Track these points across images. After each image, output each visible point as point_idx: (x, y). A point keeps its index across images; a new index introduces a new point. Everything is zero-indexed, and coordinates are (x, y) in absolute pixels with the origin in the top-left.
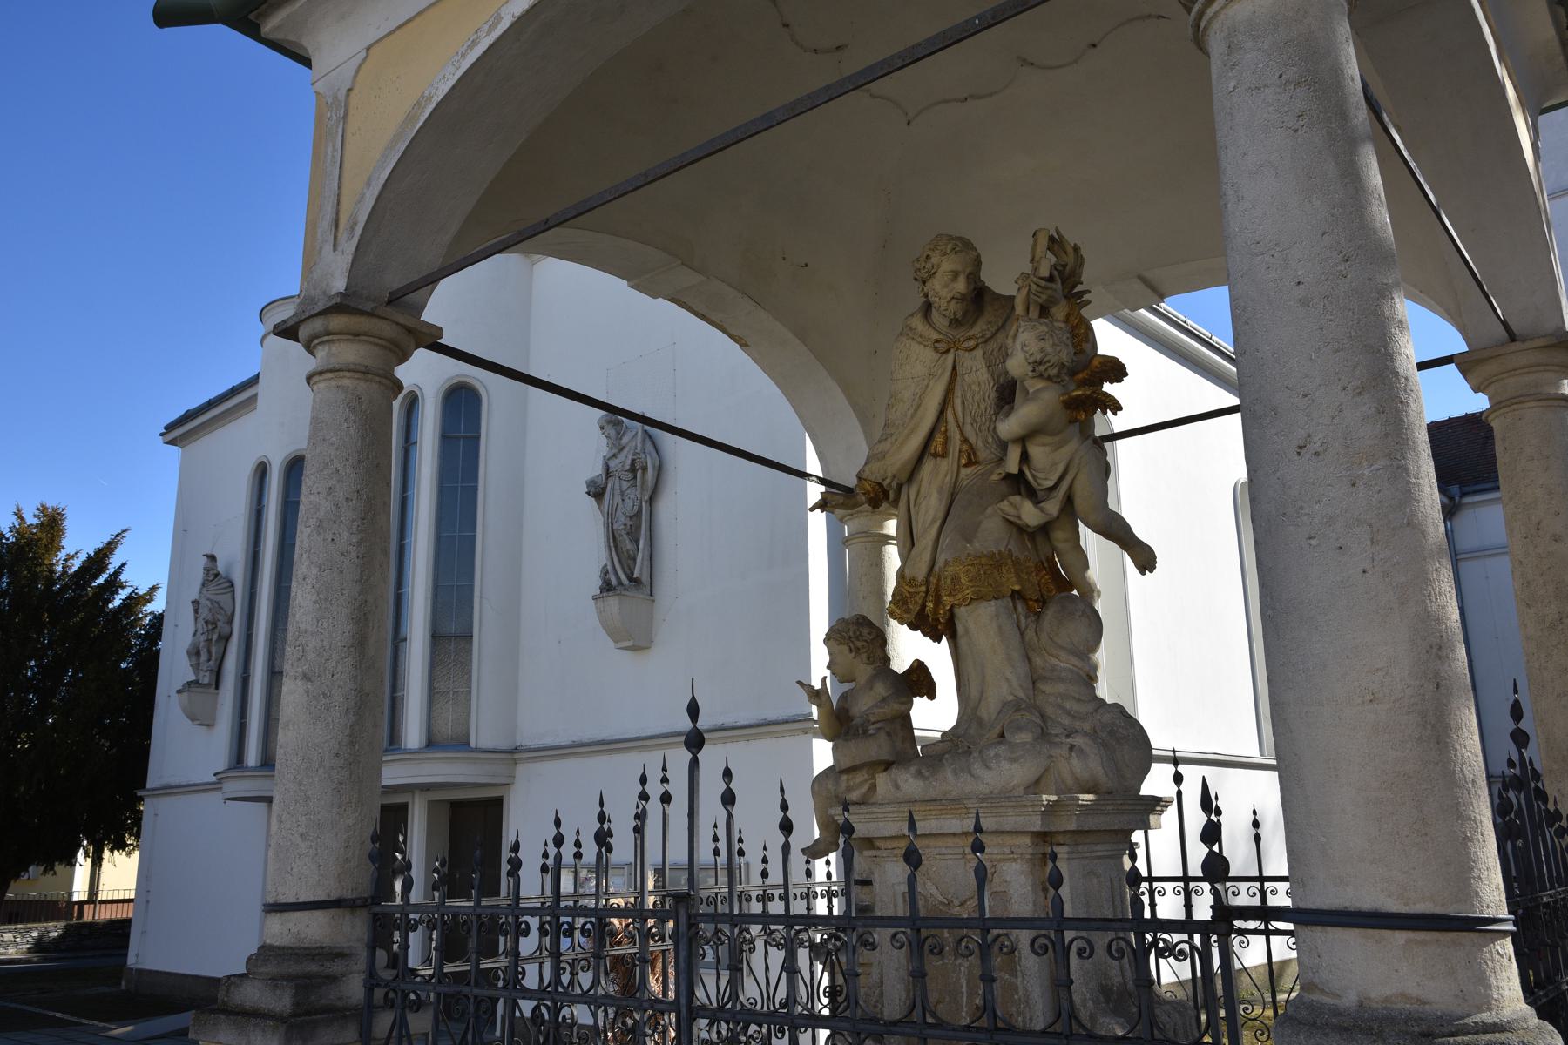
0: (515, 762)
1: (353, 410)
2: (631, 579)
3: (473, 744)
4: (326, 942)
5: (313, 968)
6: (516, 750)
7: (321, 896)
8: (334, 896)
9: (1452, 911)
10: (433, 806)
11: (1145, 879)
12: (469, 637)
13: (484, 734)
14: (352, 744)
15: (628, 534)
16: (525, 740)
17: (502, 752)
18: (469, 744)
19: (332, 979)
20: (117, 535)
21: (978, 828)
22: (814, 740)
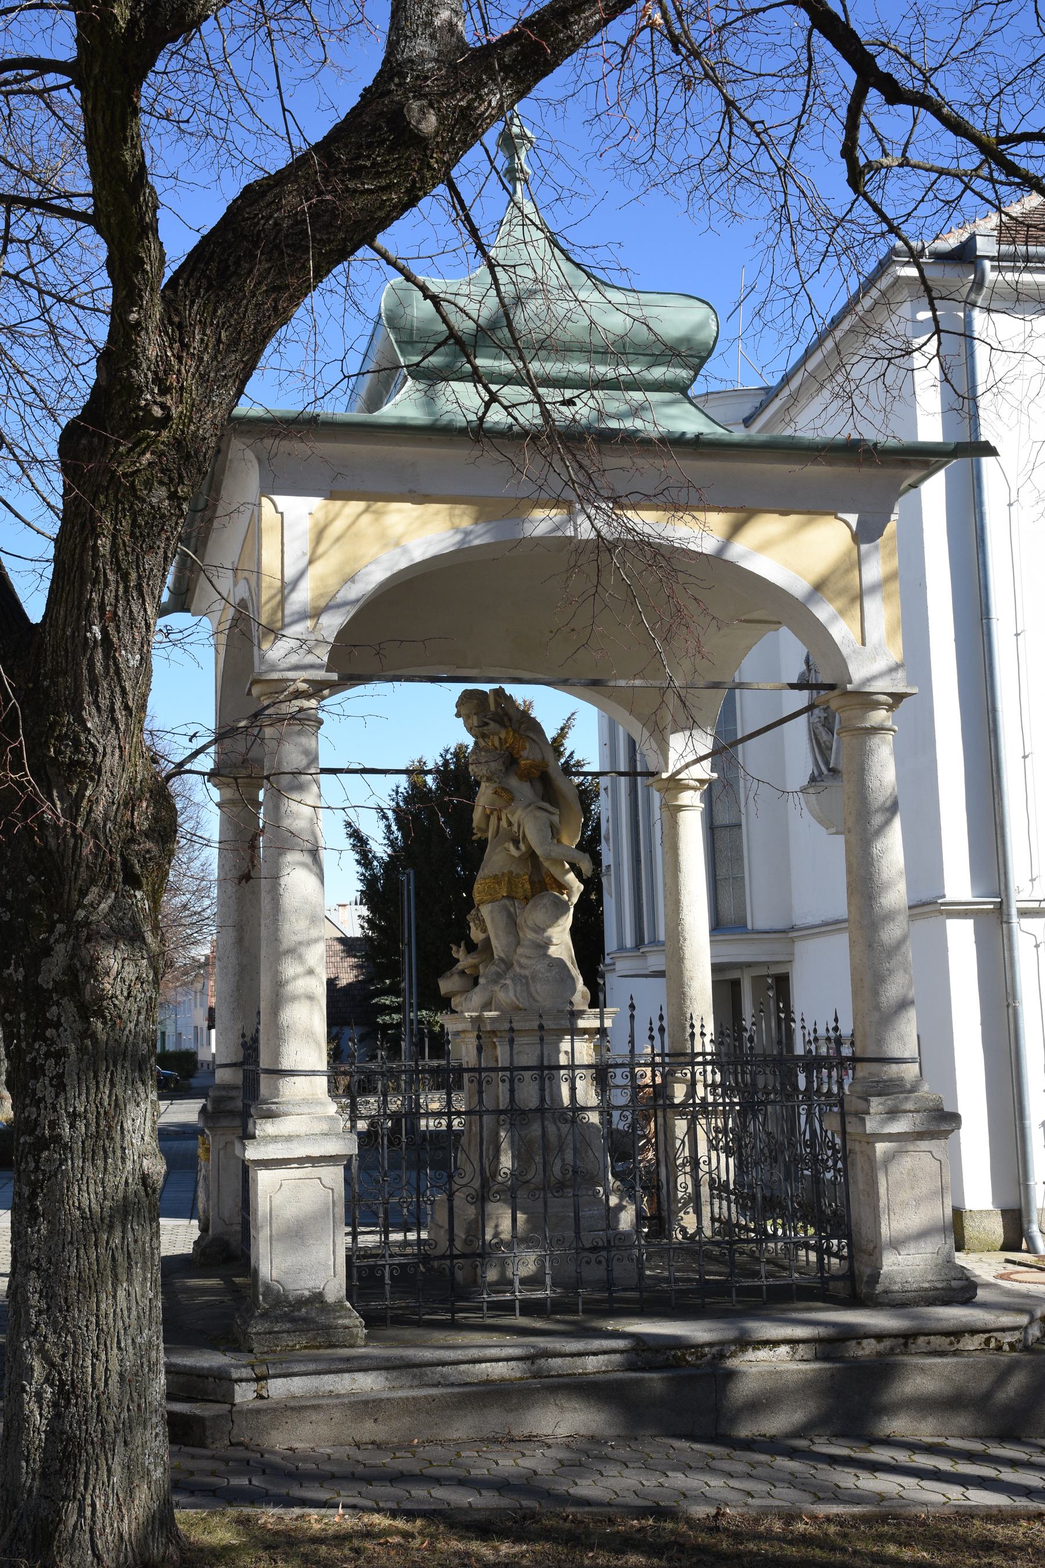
0: (793, 940)
1: (230, 824)
2: (830, 770)
3: (749, 927)
4: (232, 1082)
5: (224, 1093)
6: (793, 929)
7: (228, 1061)
8: (234, 1061)
9: (271, 1068)
10: (757, 980)
11: (653, 1058)
12: (739, 826)
13: (760, 917)
14: (238, 990)
15: (823, 725)
16: (799, 922)
17: (775, 932)
18: (746, 926)
19: (232, 1098)
20: (569, 719)
21: (541, 1027)
22: (948, 921)
